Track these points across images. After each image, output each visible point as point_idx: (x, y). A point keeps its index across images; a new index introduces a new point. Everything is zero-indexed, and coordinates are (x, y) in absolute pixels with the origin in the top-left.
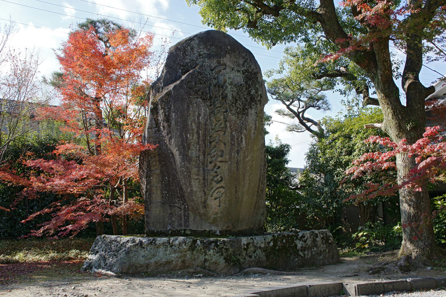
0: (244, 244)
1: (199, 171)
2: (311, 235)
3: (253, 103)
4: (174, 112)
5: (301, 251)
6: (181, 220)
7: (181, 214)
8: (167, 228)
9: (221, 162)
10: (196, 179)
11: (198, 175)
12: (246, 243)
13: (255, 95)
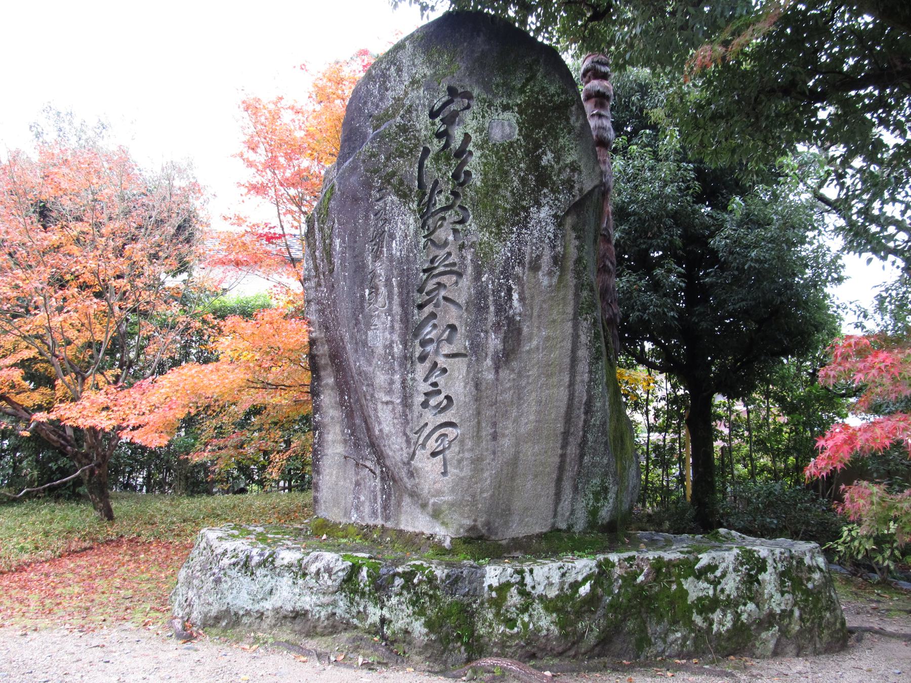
0: (490, 586)
1: (392, 382)
2: (742, 564)
3: (546, 190)
4: (338, 237)
5: (700, 613)
6: (375, 502)
7: (375, 486)
8: (350, 518)
9: (448, 356)
10: (387, 403)
11: (390, 392)
12: (495, 584)
13: (552, 167)
